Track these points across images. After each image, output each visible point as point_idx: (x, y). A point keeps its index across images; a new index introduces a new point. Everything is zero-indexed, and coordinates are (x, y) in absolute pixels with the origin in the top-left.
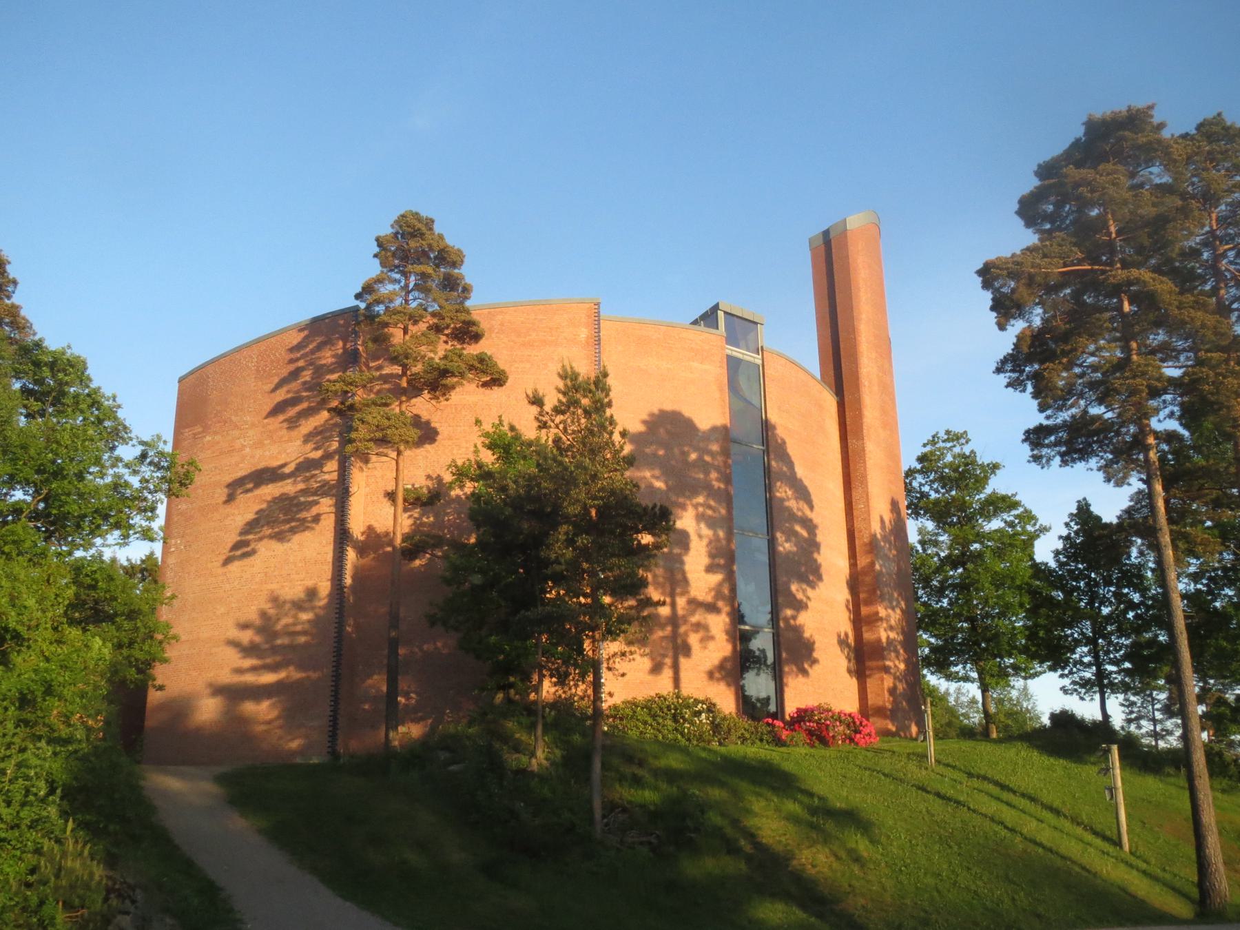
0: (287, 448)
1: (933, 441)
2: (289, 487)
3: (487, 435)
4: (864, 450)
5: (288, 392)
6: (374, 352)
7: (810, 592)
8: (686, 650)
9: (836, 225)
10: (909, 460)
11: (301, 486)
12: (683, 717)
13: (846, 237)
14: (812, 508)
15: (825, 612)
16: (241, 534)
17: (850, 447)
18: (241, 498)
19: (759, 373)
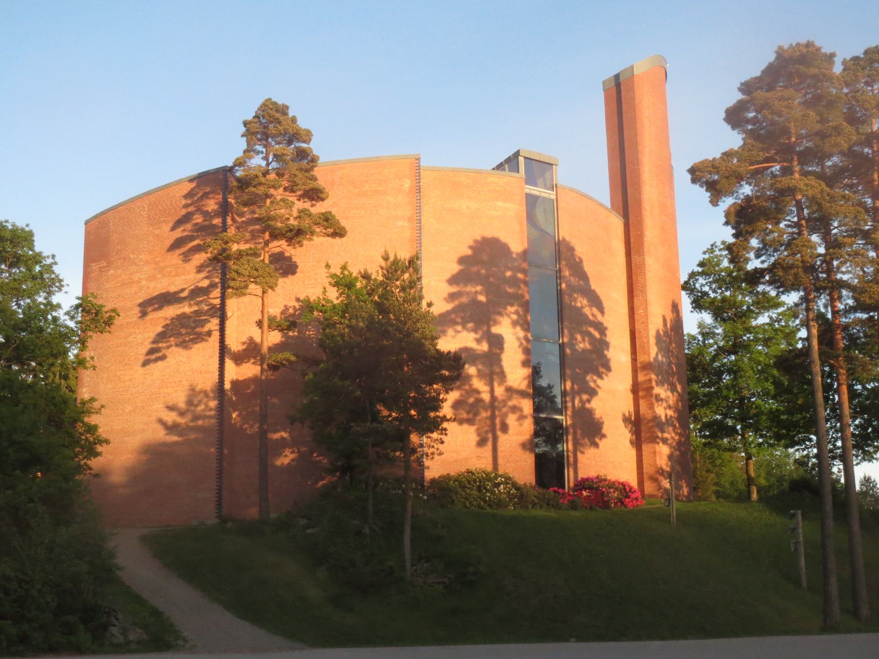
0: (186, 275)
1: (711, 250)
2: (186, 309)
3: (333, 276)
4: (644, 265)
5: (184, 231)
6: (245, 206)
7: (599, 382)
8: (505, 428)
9: (626, 70)
10: (688, 265)
11: (196, 308)
12: (485, 488)
13: (633, 82)
14: (602, 310)
15: (612, 397)
16: (153, 342)
17: (633, 262)
18: (151, 316)
19: (553, 207)
